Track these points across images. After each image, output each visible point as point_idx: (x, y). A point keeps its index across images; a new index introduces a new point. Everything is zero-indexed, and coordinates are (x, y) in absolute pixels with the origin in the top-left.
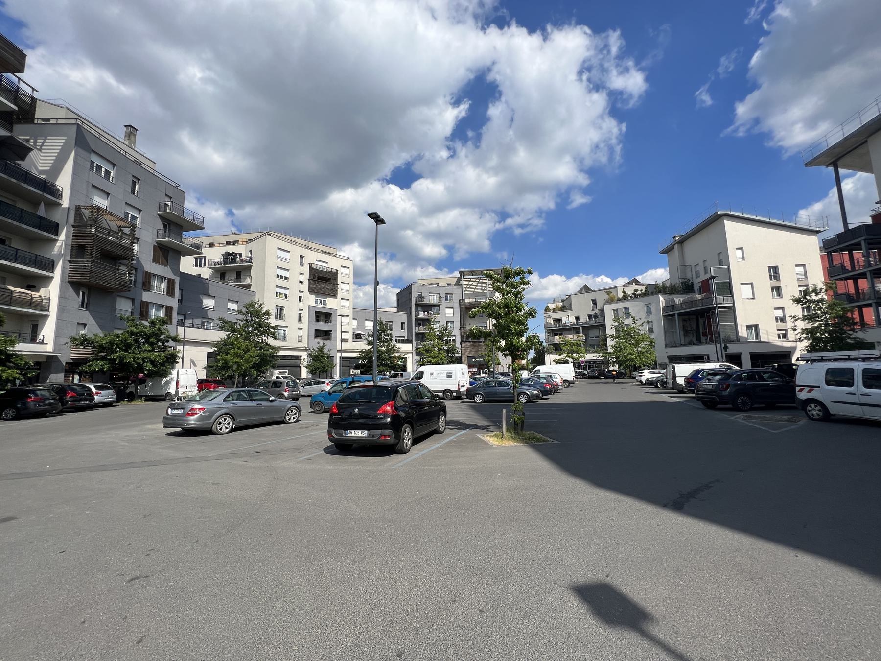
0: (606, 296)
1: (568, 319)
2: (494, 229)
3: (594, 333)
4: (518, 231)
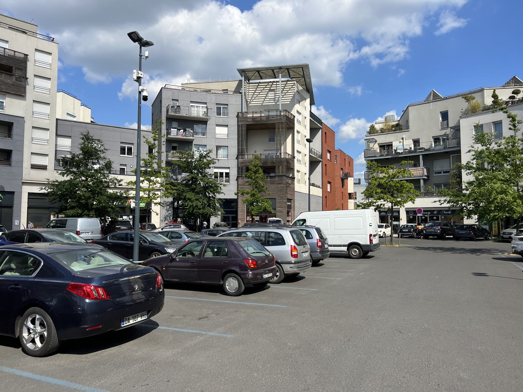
0: (464, 105)
1: (402, 143)
2: (348, 59)
3: (440, 166)
4: (375, 62)
